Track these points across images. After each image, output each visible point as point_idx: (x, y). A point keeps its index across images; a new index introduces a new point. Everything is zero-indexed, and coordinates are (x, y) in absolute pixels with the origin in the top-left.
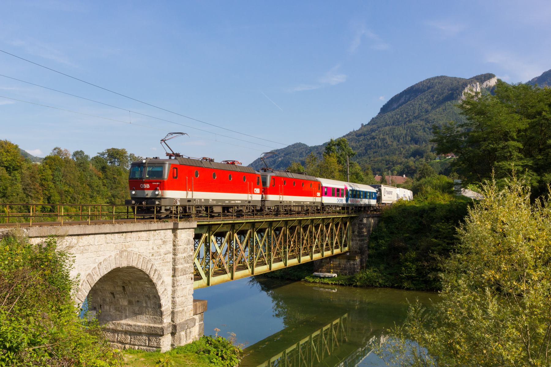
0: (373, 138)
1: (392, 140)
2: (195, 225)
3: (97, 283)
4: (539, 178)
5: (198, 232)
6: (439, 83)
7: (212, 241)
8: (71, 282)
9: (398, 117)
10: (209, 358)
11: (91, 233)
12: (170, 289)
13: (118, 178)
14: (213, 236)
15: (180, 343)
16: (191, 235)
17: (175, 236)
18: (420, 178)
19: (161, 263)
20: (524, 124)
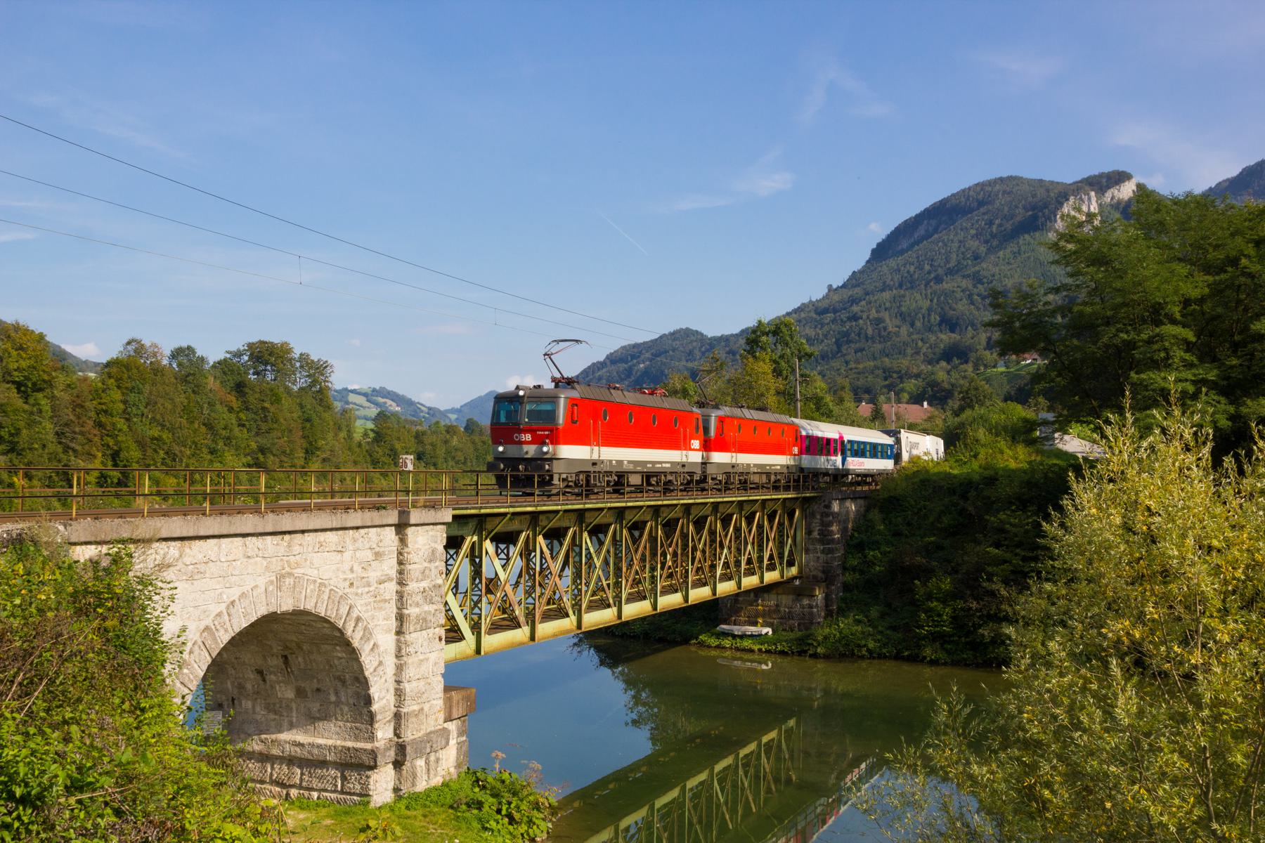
0: (855, 318)
1: (898, 322)
2: (447, 515)
3: (224, 648)
5: (456, 532)
6: (1004, 192)
7: (487, 553)
8: (165, 647)
9: (912, 269)
10: (480, 820)
11: (210, 533)
12: (390, 662)
13: (272, 409)
14: (488, 541)
15: (414, 785)
16: (439, 539)
17: (403, 541)
18: (962, 409)
19: (370, 603)
20: (1197, 286)
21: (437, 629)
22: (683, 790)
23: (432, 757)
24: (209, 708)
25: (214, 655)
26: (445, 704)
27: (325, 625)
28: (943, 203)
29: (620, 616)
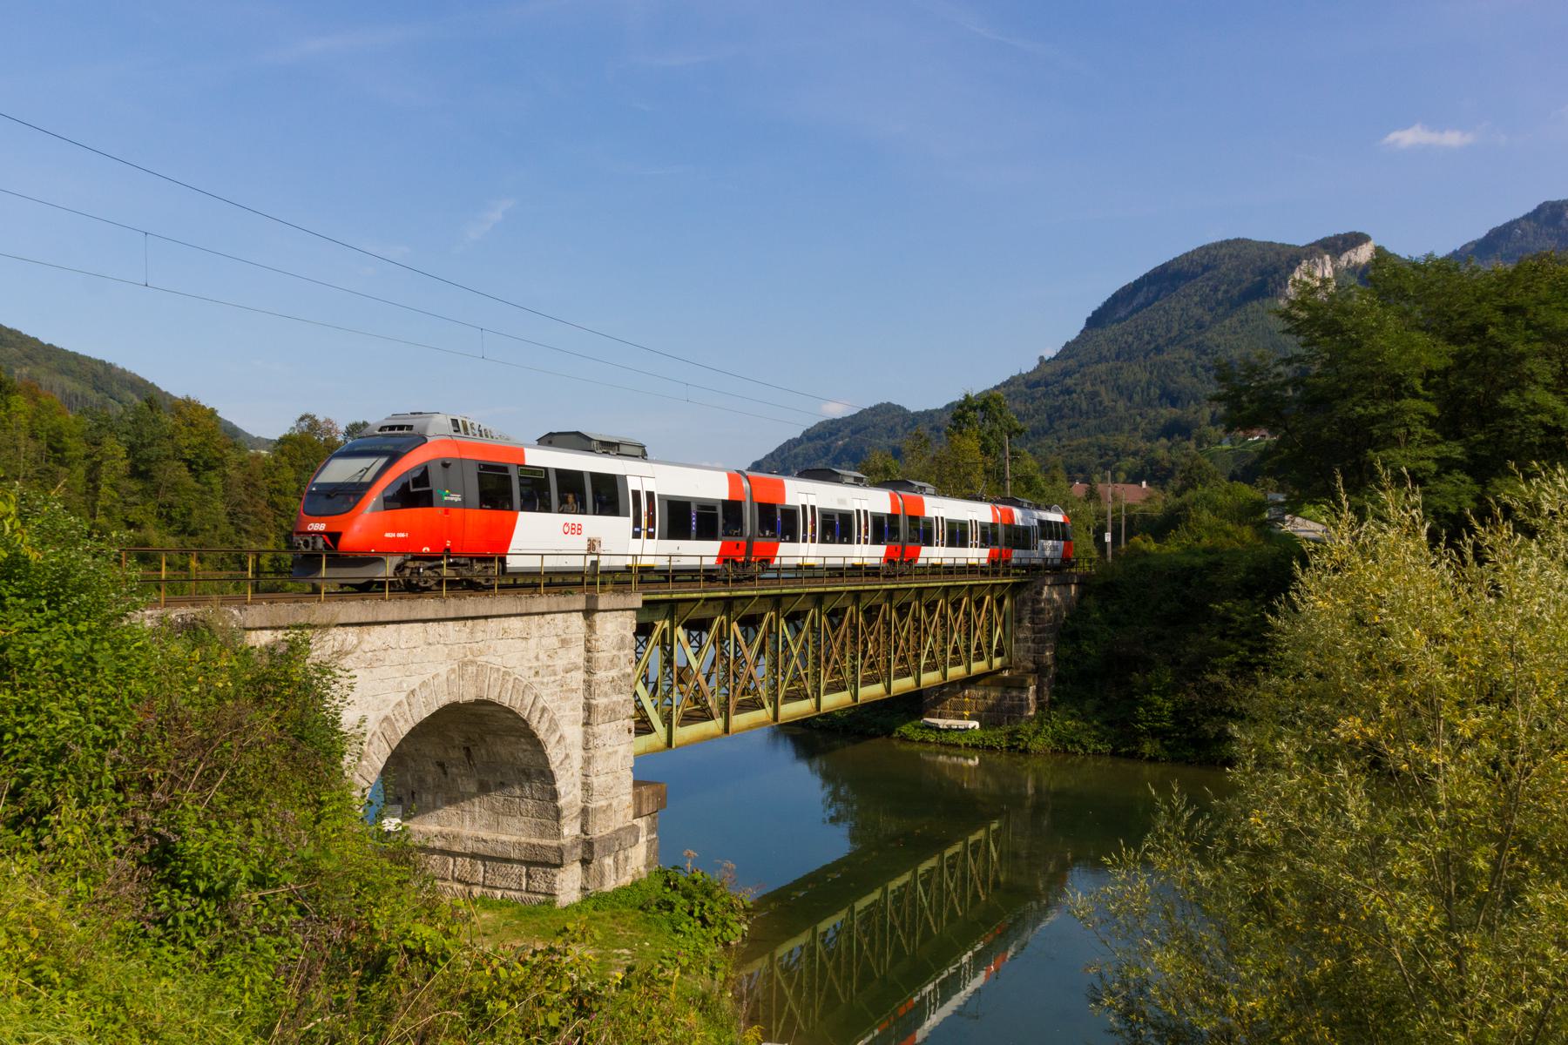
2: (637, 601)
4: (1477, 489)
8: (344, 738)
10: (671, 922)
12: (577, 755)
14: (680, 628)
15: (601, 884)
17: (591, 627)
18: (1183, 489)
20: (1434, 354)
23: (621, 856)
25: (394, 746)
26: (634, 799)
28: (1164, 267)
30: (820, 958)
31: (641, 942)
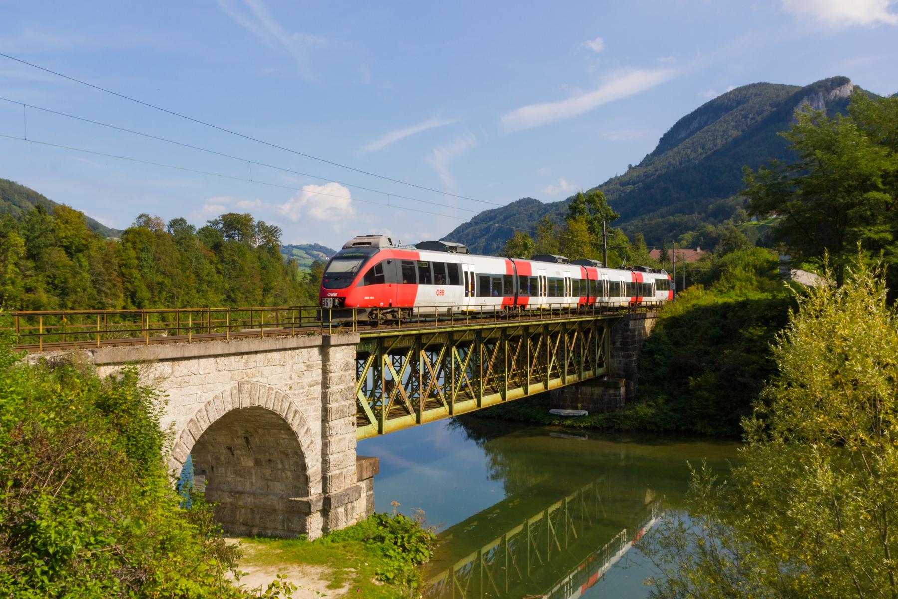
2: (356, 339)
3: (205, 432)
5: (364, 349)
6: (756, 95)
7: (385, 364)
8: (161, 434)
10: (382, 549)
11: (192, 355)
13: (240, 261)
15: (337, 525)
18: (725, 252)
19: (304, 400)
21: (351, 418)
22: (526, 525)
24: (196, 473)
25: (197, 438)
26: (357, 468)
27: (274, 416)
29: (479, 405)
30: (509, 553)
31: (362, 562)
